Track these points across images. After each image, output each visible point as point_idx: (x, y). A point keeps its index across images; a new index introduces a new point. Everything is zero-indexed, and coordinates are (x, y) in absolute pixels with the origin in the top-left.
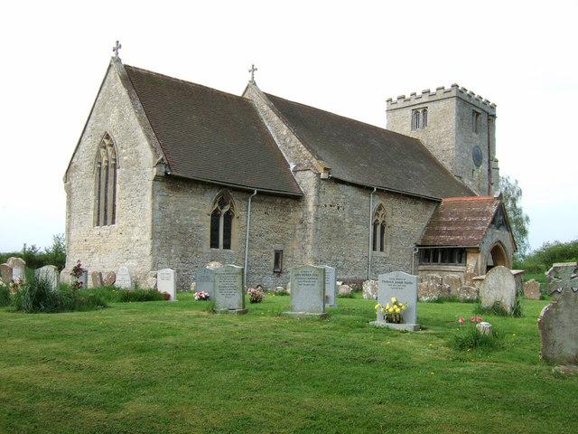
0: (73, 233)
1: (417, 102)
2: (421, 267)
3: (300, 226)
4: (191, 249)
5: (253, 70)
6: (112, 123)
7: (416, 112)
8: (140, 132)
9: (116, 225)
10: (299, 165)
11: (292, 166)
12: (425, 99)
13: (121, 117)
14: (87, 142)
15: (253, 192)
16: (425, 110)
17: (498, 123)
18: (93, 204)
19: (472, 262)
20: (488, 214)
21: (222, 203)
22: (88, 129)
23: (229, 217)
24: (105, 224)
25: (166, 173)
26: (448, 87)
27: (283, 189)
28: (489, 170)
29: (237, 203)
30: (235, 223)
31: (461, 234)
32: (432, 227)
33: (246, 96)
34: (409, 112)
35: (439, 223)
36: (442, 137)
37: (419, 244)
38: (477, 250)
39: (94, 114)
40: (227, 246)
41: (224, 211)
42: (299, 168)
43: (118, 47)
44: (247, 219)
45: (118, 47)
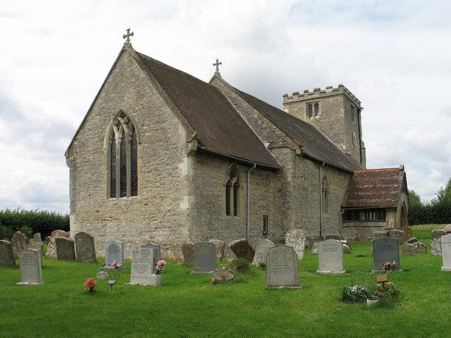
0: (79, 205)
1: (310, 97)
2: (345, 225)
3: (279, 195)
4: (214, 217)
5: (217, 64)
6: (127, 102)
7: (310, 106)
8: (167, 110)
9: (138, 197)
10: (271, 143)
11: (267, 145)
12: (316, 96)
13: (140, 96)
14: (96, 119)
15: (252, 166)
16: (317, 105)
17: (363, 113)
18: (106, 177)
19: (391, 220)
20: (396, 181)
21: (232, 175)
22: (96, 108)
23: (236, 187)
24: (122, 196)
25: (198, 148)
26: (336, 87)
27: (269, 164)
28: (360, 150)
29: (242, 178)
30: (241, 193)
31: (379, 197)
32: (352, 190)
33: (212, 84)
34: (304, 105)
35: (358, 190)
36: (327, 122)
37: (344, 206)
38: (395, 209)
39: (103, 94)
40: (235, 214)
41: (233, 182)
42: (274, 146)
43: (129, 34)
44: (251, 189)
45: (129, 34)
